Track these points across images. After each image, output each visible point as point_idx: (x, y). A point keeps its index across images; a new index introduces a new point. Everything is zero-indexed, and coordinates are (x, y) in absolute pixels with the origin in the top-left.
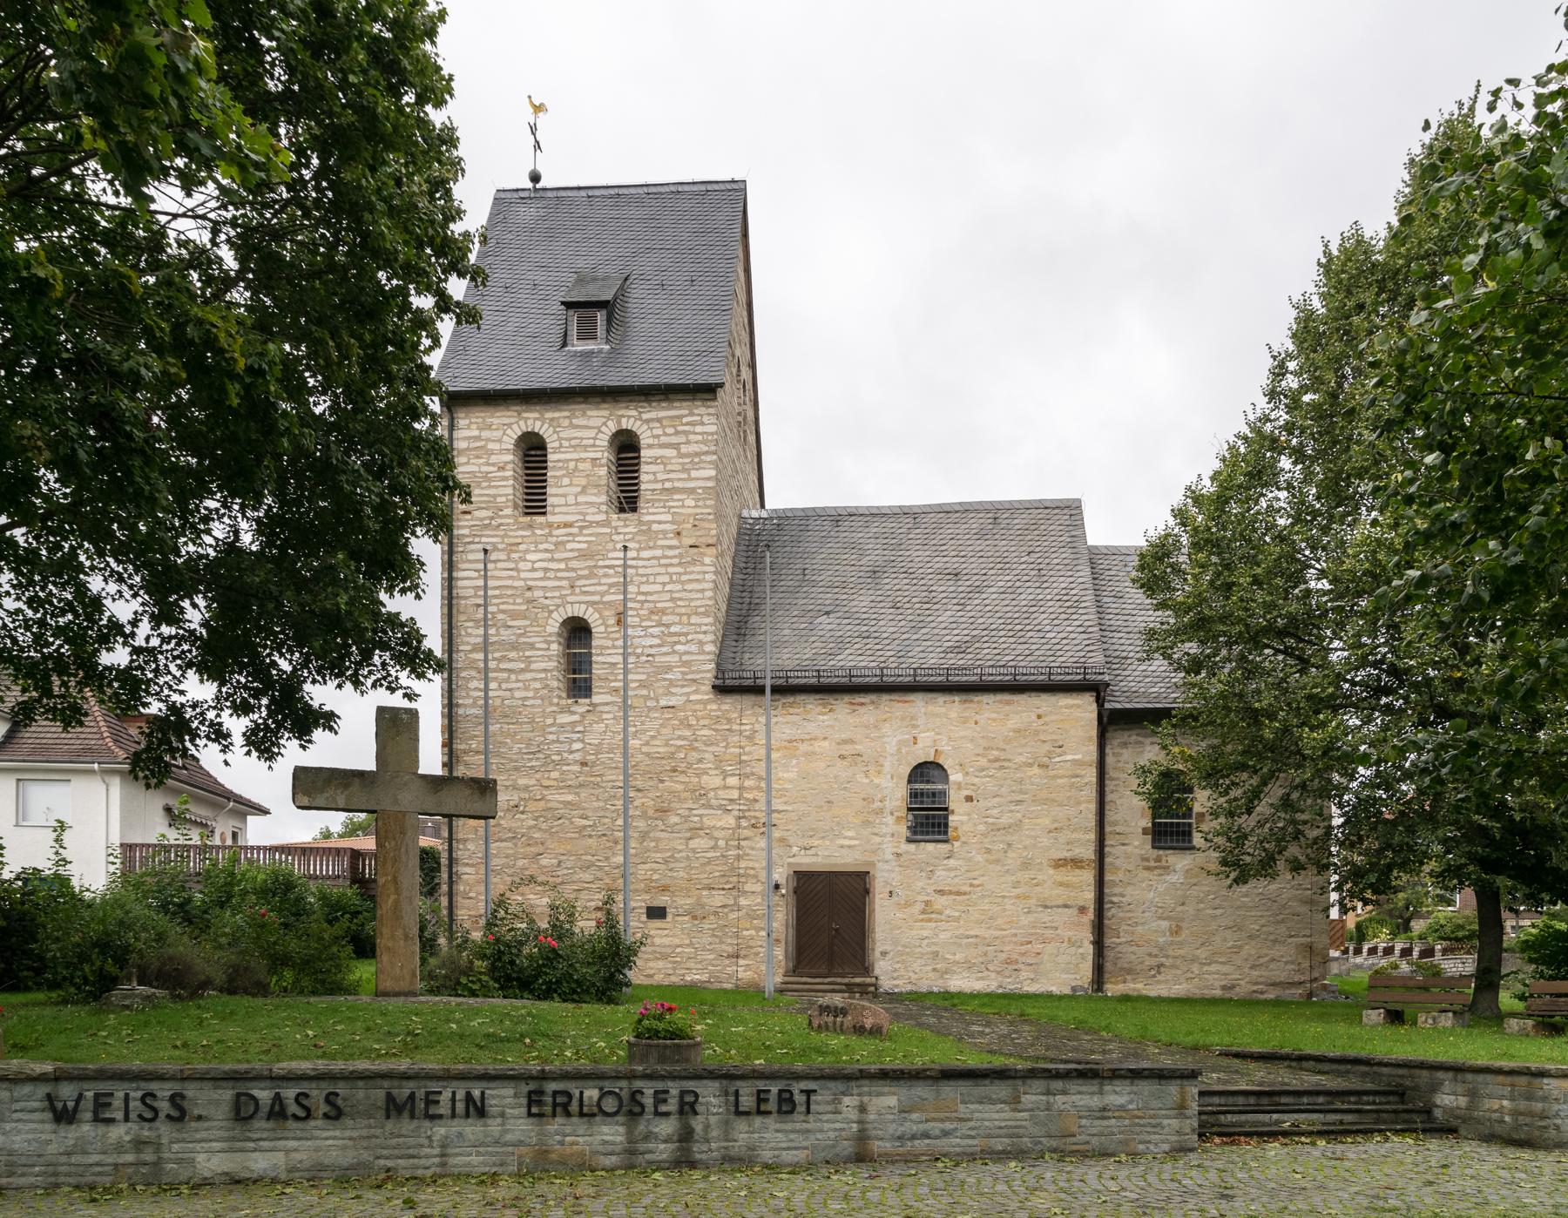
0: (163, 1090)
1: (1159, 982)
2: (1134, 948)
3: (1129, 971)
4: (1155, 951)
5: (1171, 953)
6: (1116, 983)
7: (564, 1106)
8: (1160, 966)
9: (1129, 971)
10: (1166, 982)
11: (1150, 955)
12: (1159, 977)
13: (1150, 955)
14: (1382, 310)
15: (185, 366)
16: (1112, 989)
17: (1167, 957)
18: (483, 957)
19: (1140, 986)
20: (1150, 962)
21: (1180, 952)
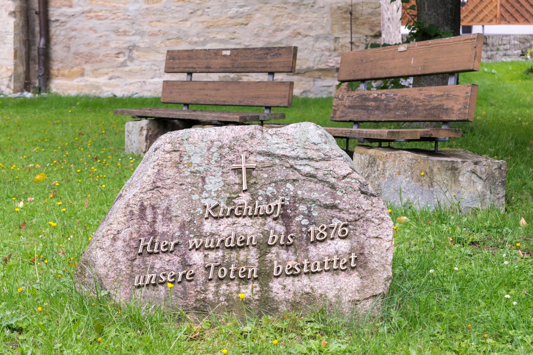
0: (305, 270)
1: (131, 73)
2: (94, 23)
3: (89, 58)
4: (124, 26)
5: (146, 28)
6: (70, 77)
7: (337, 263)
8: (132, 48)
9: (89, 58)
10: (142, 72)
11: (116, 31)
12: (132, 66)
13: (116, 31)
14: (176, 349)
15: (14, 87)
16: (62, 85)
17: (141, 33)
18: (88, 230)
19: (102, 80)
20: (117, 42)
21: (160, 26)
